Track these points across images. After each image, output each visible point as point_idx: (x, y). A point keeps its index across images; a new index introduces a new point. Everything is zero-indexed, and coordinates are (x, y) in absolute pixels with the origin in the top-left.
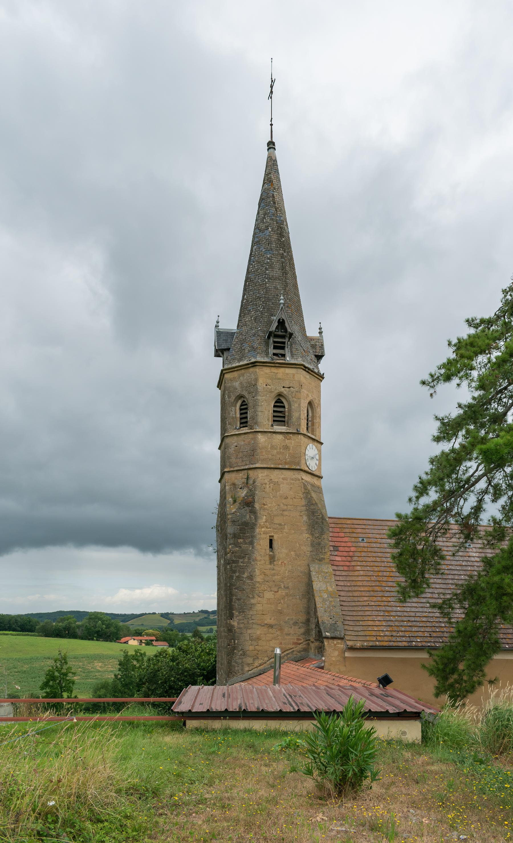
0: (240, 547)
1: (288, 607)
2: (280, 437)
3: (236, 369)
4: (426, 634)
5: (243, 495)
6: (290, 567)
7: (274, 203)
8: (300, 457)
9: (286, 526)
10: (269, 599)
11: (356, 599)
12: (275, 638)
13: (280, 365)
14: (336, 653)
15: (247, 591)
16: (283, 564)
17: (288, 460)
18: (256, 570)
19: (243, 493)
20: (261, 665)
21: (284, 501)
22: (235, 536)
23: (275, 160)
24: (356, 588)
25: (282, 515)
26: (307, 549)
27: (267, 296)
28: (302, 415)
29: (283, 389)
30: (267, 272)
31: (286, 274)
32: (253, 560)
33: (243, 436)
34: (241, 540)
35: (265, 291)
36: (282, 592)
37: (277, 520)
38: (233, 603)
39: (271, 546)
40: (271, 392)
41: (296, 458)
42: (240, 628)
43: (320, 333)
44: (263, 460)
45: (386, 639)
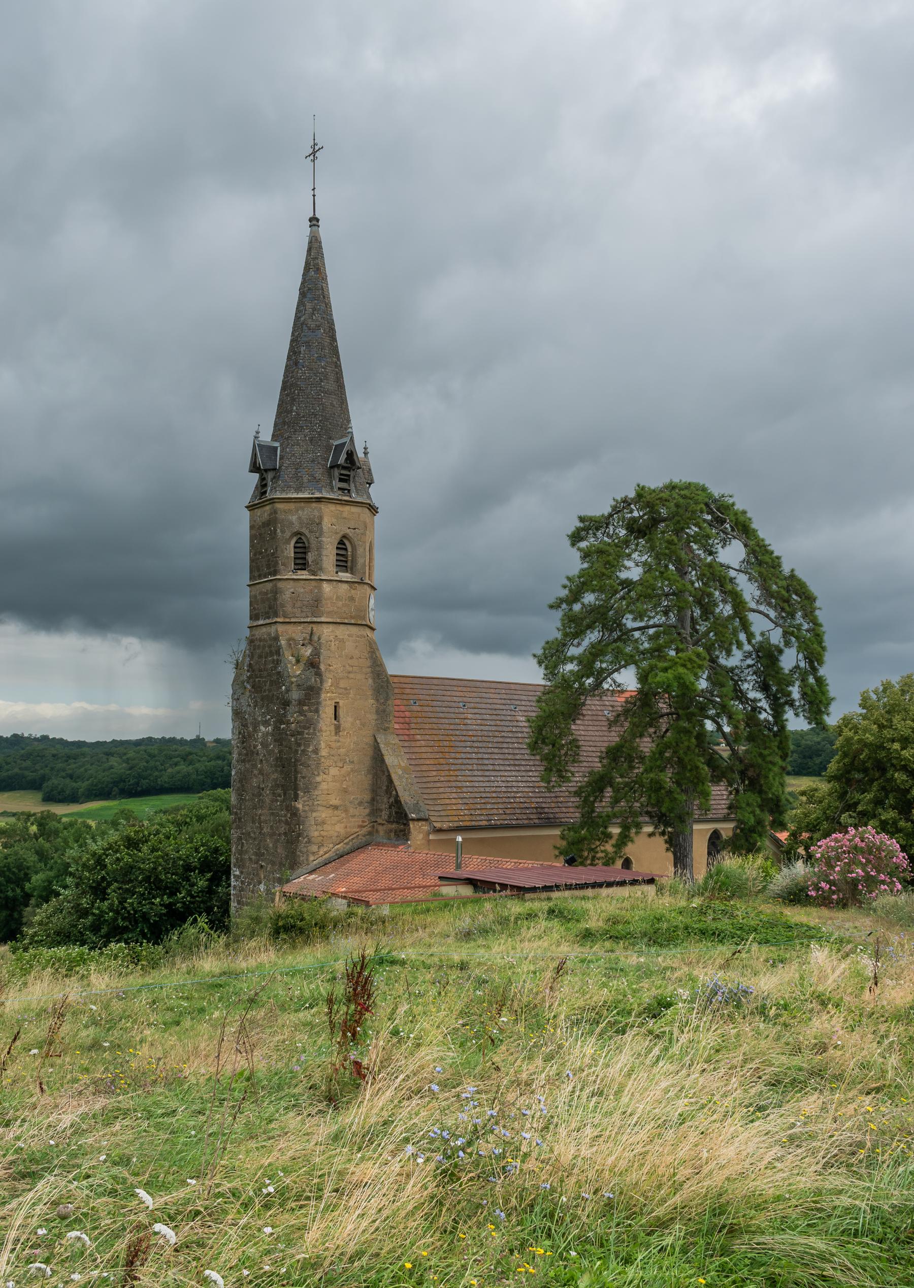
2: (345, 586)
4: (501, 812)
8: (365, 611)
11: (425, 774)
12: (339, 822)
14: (421, 836)
19: (308, 652)
20: (326, 853)
21: (350, 661)
22: (301, 703)
24: (422, 762)
26: (372, 717)
29: (348, 531)
36: (347, 768)
37: (342, 685)
40: (337, 533)
42: (304, 811)
44: (329, 614)
45: (467, 818)
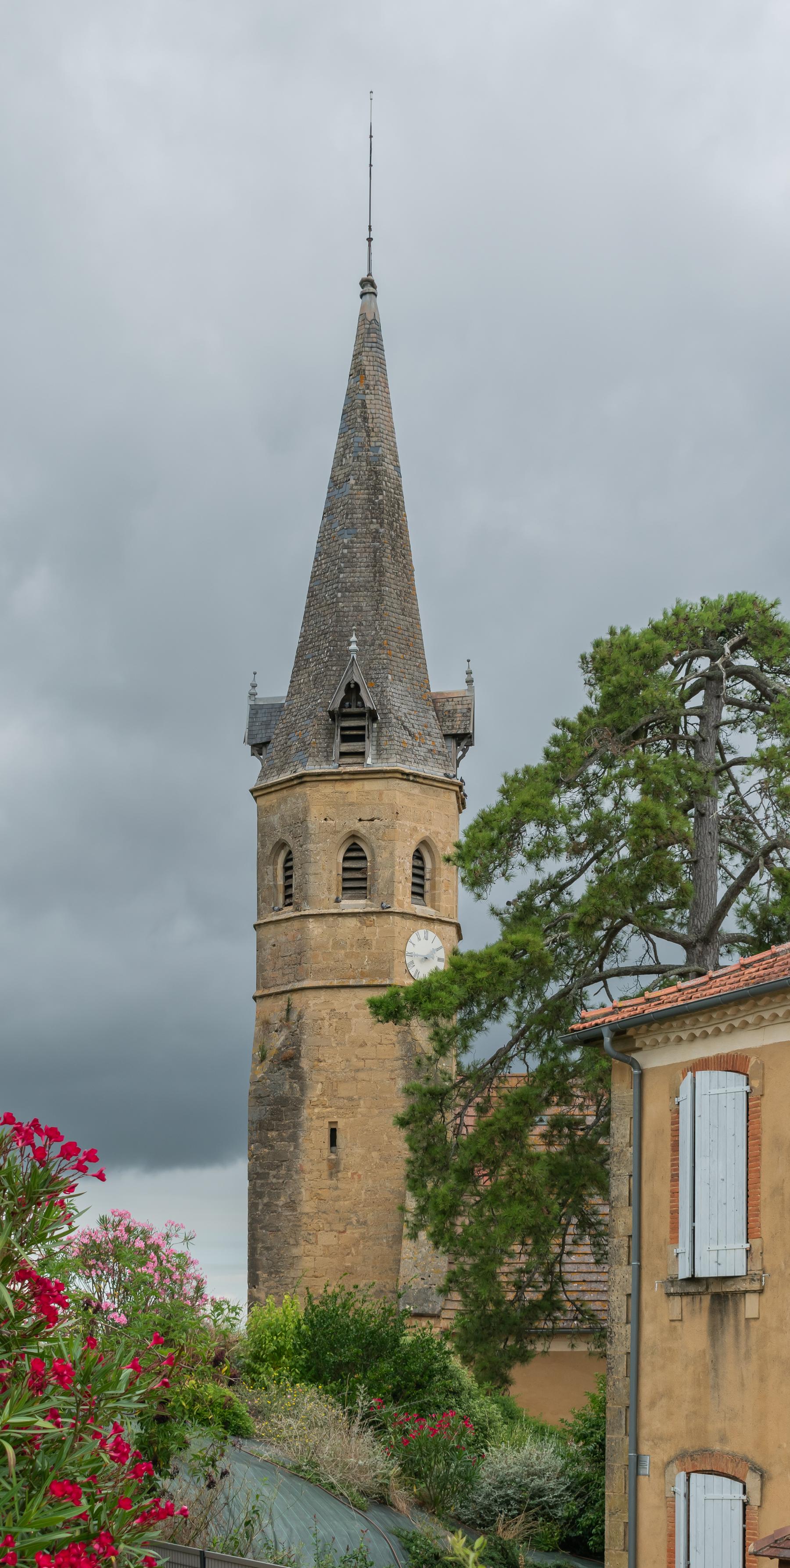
0: (272, 1147)
1: (364, 1261)
2: (353, 922)
3: (273, 789)
5: (278, 1044)
6: (370, 1182)
7: (365, 419)
9: (362, 1102)
10: (328, 1247)
13: (352, 777)
15: (285, 1232)
16: (356, 1177)
17: (368, 968)
18: (303, 1190)
19: (278, 1040)
21: (358, 1051)
23: (375, 321)
25: (354, 1079)
27: (338, 629)
28: (397, 874)
30: (341, 576)
31: (382, 573)
32: (296, 1172)
33: (284, 925)
34: (274, 1134)
35: (334, 618)
36: (353, 1233)
37: (344, 1091)
38: (257, 1257)
39: (333, 1142)
40: (336, 832)
41: (385, 962)
43: (470, 682)
